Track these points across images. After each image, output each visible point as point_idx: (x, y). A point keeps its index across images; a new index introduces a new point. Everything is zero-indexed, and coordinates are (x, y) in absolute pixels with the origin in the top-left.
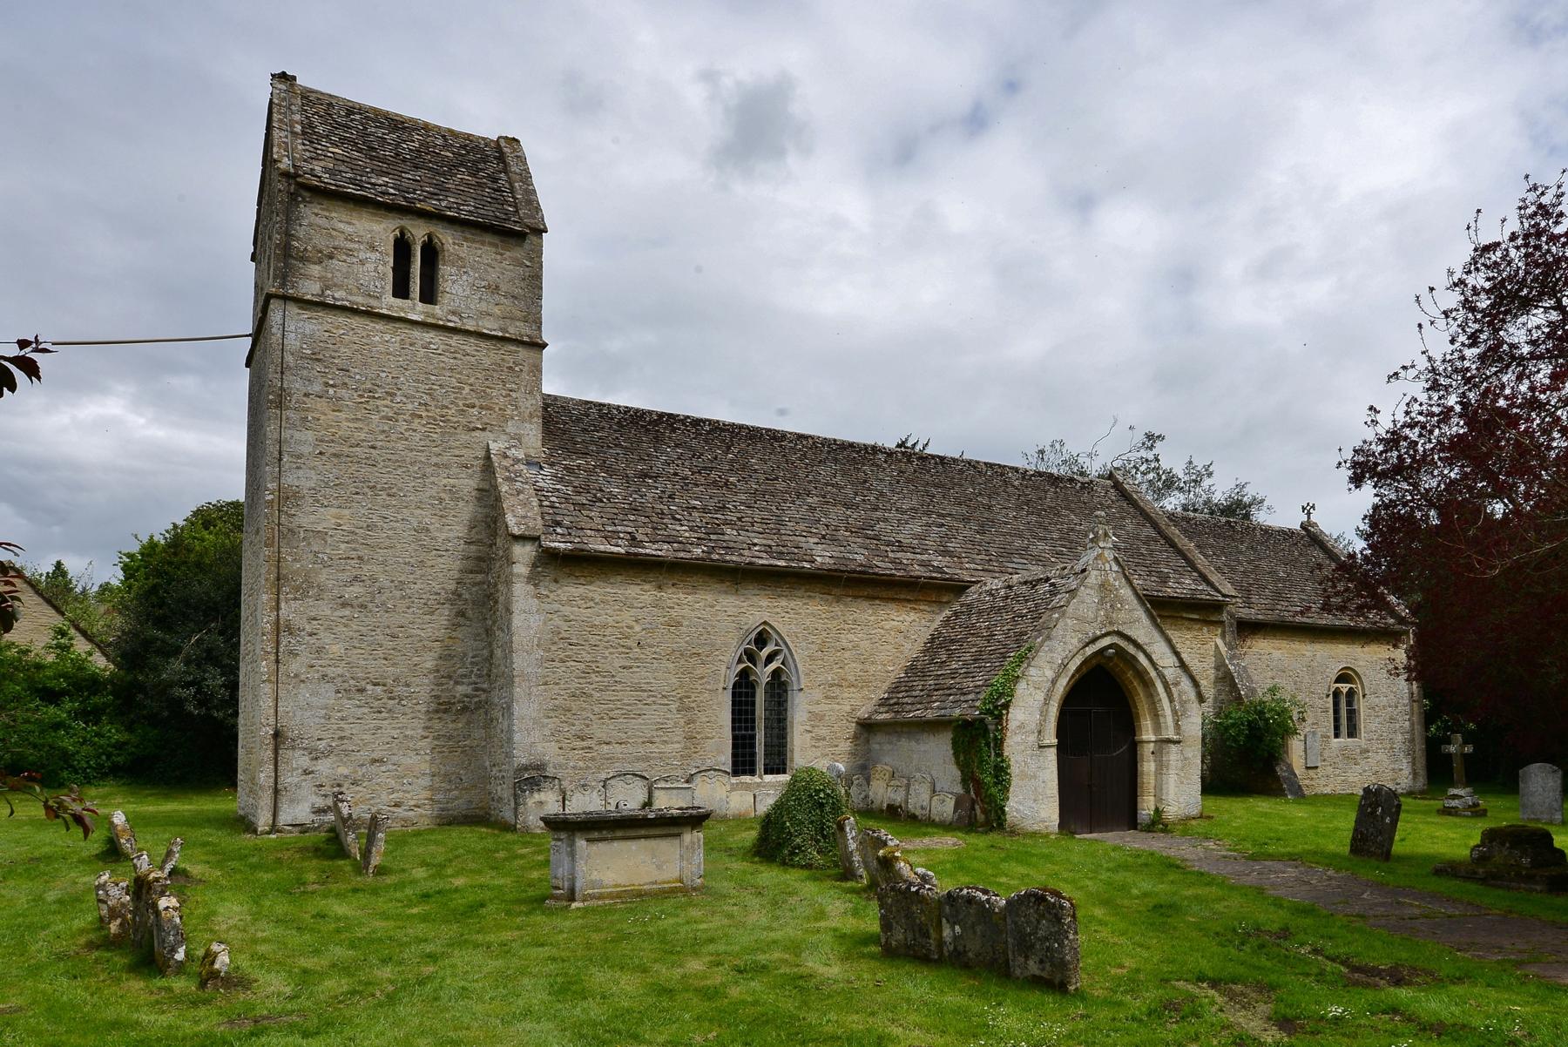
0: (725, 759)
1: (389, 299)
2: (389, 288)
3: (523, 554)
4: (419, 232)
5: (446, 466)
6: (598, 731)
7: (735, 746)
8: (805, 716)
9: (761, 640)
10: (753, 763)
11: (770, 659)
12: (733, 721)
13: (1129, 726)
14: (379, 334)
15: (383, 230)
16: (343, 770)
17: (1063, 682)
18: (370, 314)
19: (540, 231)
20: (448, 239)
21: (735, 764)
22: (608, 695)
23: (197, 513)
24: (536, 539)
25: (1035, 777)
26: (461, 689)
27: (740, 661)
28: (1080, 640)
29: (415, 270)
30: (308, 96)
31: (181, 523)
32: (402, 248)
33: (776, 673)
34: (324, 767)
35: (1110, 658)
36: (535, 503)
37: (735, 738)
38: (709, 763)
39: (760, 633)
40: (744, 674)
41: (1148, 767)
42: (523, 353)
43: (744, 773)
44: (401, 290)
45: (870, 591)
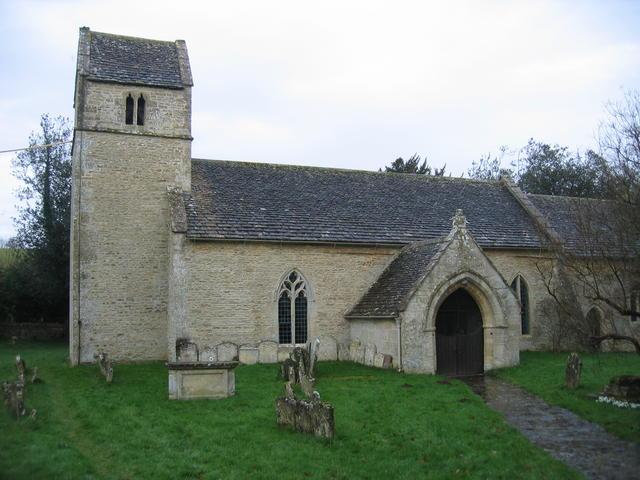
0: (276, 336)
2: (124, 120)
4: (136, 92)
5: (148, 199)
6: (215, 323)
7: (280, 329)
8: (317, 314)
9: (293, 277)
10: (290, 338)
11: (298, 286)
12: (280, 317)
13: (480, 321)
16: (106, 339)
17: (437, 299)
18: (116, 132)
20: (147, 92)
21: (281, 338)
22: (218, 306)
23: (404, 169)
25: (421, 347)
28: (447, 277)
29: (135, 111)
30: (94, 35)
32: (130, 101)
33: (301, 293)
34: (98, 337)
35: (466, 285)
36: (185, 215)
37: (280, 325)
38: (267, 337)
39: (293, 274)
40: (285, 294)
41: (488, 341)
42: (182, 143)
43: (285, 342)
44: (129, 121)
45: (349, 250)
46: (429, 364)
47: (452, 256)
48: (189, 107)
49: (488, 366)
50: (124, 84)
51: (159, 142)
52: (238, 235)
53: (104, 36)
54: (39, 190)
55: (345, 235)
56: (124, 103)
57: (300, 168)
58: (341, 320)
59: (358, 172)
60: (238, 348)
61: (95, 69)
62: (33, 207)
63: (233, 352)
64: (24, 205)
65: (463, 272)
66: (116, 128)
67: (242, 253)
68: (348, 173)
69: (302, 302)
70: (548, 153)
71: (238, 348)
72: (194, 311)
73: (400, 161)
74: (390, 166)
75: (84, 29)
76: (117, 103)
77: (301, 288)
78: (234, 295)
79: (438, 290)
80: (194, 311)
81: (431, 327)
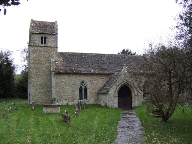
0: (79, 98)
1: (40, 44)
3: (53, 73)
4: (44, 36)
6: (63, 94)
9: (83, 82)
10: (82, 98)
11: (84, 85)
13: (131, 94)
14: (40, 49)
15: (40, 36)
17: (118, 88)
18: (38, 46)
19: (57, 33)
20: (46, 35)
23: (125, 52)
24: (54, 71)
26: (49, 89)
27: (80, 85)
30: (34, 21)
31: (120, 52)
32: (42, 38)
34: (34, 98)
40: (81, 87)
41: (133, 99)
42: (55, 48)
44: (42, 43)
46: (116, 105)
47: (122, 76)
48: (57, 39)
49: (133, 106)
50: (40, 34)
51: (49, 48)
52: (68, 72)
53: (37, 21)
54: (27, 60)
55: (97, 71)
56: (40, 38)
57: (88, 54)
58: (96, 93)
59: (103, 54)
60: (68, 101)
61: (34, 30)
62: (25, 64)
63: (67, 102)
64: (23, 64)
65: (125, 81)
66: (38, 45)
67: (69, 76)
68: (100, 54)
69: (86, 89)
70: (163, 47)
71: (68, 101)
72: (57, 91)
73: (124, 50)
74: (122, 51)
75: (32, 20)
76: (39, 38)
77: (85, 85)
78: (67, 87)
79: (118, 86)
80: (57, 91)
81: (117, 95)
